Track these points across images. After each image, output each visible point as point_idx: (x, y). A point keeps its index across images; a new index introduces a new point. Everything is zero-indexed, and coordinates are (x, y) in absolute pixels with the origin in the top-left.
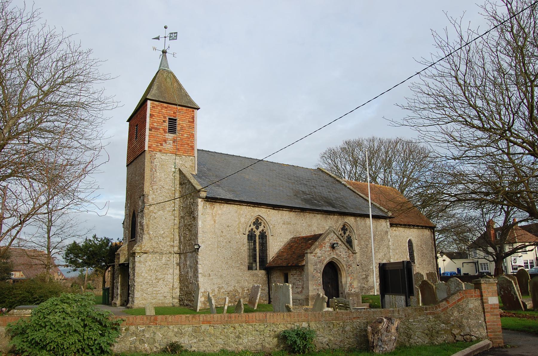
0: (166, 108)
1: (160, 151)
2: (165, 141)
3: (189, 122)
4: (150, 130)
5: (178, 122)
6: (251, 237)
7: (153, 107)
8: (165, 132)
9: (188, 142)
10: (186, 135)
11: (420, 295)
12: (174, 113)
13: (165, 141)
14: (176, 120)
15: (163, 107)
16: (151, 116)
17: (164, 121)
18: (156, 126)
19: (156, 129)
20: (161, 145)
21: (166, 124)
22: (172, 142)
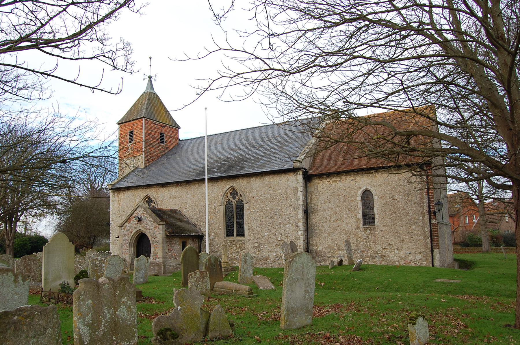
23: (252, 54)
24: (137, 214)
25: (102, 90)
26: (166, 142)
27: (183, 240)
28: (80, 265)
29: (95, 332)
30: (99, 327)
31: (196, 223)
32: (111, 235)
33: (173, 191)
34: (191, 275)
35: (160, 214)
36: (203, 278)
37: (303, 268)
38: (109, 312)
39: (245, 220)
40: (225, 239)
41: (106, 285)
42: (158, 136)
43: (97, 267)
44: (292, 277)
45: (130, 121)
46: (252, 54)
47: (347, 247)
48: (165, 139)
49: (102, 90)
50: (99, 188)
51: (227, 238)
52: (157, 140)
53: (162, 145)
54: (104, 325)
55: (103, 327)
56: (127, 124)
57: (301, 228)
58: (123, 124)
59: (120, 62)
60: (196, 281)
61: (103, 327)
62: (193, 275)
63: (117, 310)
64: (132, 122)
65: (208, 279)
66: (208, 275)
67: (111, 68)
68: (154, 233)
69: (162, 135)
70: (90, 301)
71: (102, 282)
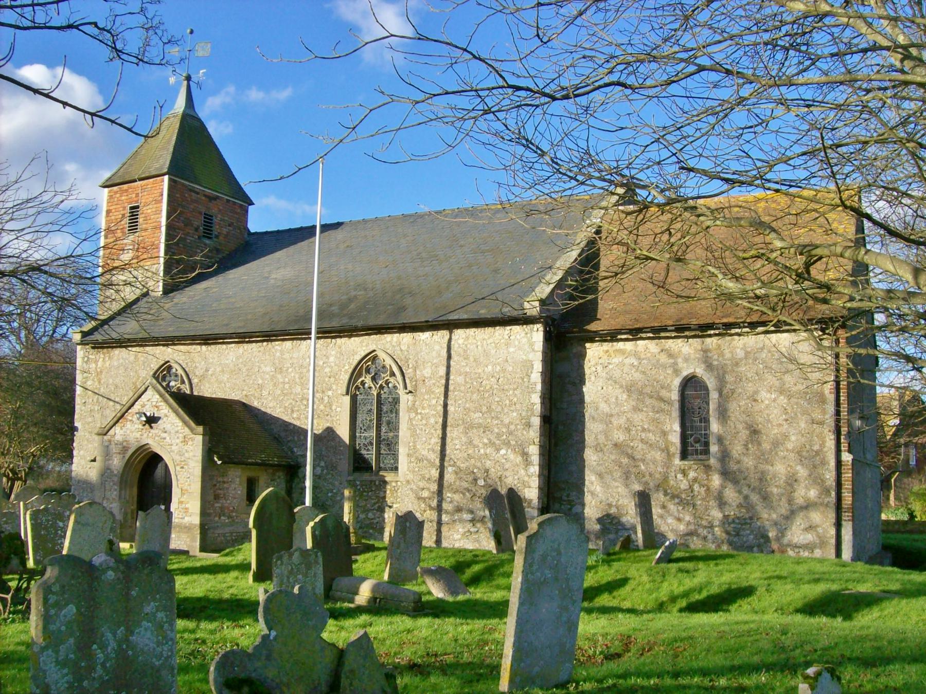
0: (126, 191)
7: (111, 197)
23: (465, 50)
24: (143, 406)
25: (113, 122)
26: (217, 237)
27: (252, 474)
28: (6, 523)
29: (80, 680)
30: (91, 668)
31: (283, 434)
32: (75, 453)
33: (231, 353)
34: (280, 558)
35: (195, 408)
36: (309, 567)
37: (559, 553)
38: (114, 634)
39: (401, 434)
40: (351, 478)
41: (110, 573)
42: (198, 222)
43: (46, 528)
44: (532, 574)
45: (135, 181)
46: (465, 50)
47: (643, 509)
48: (216, 229)
49: (113, 122)
50: (45, 339)
51: (357, 475)
52: (197, 229)
53: (207, 242)
54: (103, 665)
55: (99, 670)
56: (125, 186)
57: (535, 459)
58: (115, 188)
59: (132, 42)
60: (291, 572)
61: (99, 670)
62: (285, 558)
63: (132, 633)
64: (139, 183)
65: (319, 570)
66: (321, 560)
67: (107, 52)
68: (180, 454)
69: (208, 219)
70: (71, 609)
71: (101, 565)
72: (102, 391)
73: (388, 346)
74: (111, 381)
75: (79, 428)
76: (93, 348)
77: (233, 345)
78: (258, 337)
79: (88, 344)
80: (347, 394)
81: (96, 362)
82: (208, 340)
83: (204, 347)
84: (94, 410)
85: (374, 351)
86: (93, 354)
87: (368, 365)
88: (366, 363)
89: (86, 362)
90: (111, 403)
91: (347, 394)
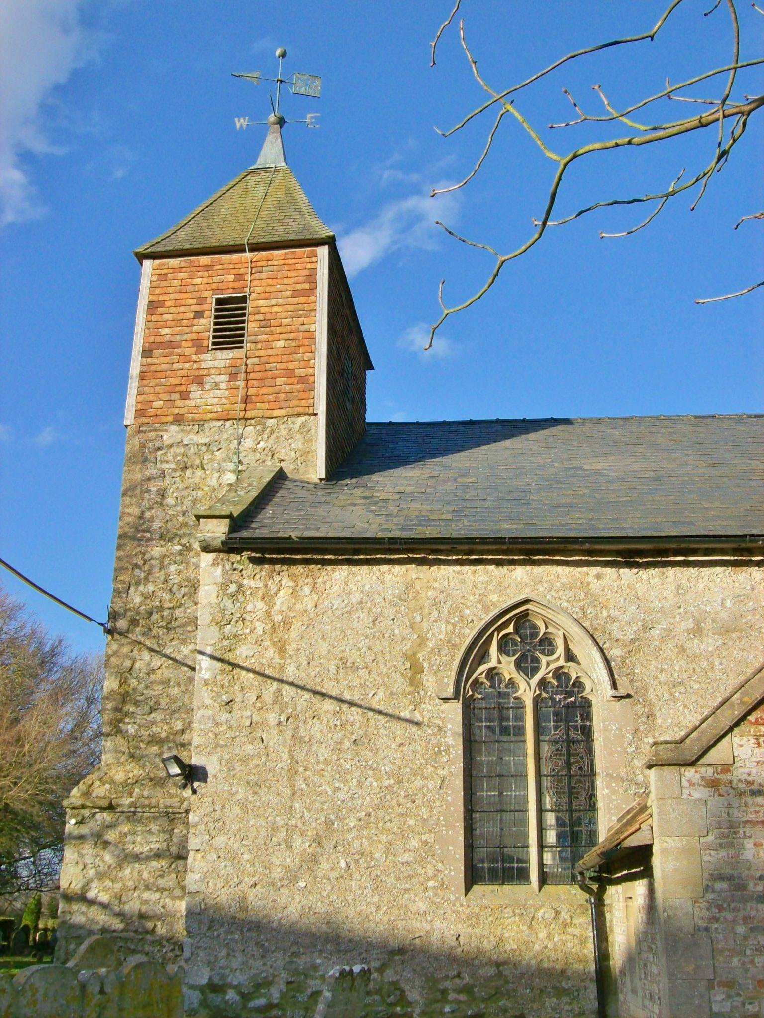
0: (207, 268)
1: (178, 419)
2: (199, 381)
3: (296, 293)
4: (147, 353)
5: (250, 305)
6: (485, 720)
7: (162, 277)
8: (200, 348)
9: (291, 366)
10: (281, 344)
11: (379, 556)
12: (239, 277)
13: (199, 381)
14: (244, 300)
15: (194, 270)
16: (152, 306)
17: (199, 314)
18: (168, 338)
19: (170, 345)
20: (185, 395)
21: (208, 323)
22: (225, 378)
45: (239, 249)
56: (205, 260)
72: (291, 673)
73: (549, 588)
74: (324, 647)
75: (211, 771)
76: (252, 560)
77: (719, 569)
78: (723, 552)
79: (238, 551)
80: (456, 697)
81: (268, 598)
82: (636, 551)
83: (624, 571)
84: (264, 723)
85: (527, 601)
86: (255, 578)
87: (519, 631)
88: (499, 629)
89: (233, 596)
90: (328, 706)
91: (456, 697)
